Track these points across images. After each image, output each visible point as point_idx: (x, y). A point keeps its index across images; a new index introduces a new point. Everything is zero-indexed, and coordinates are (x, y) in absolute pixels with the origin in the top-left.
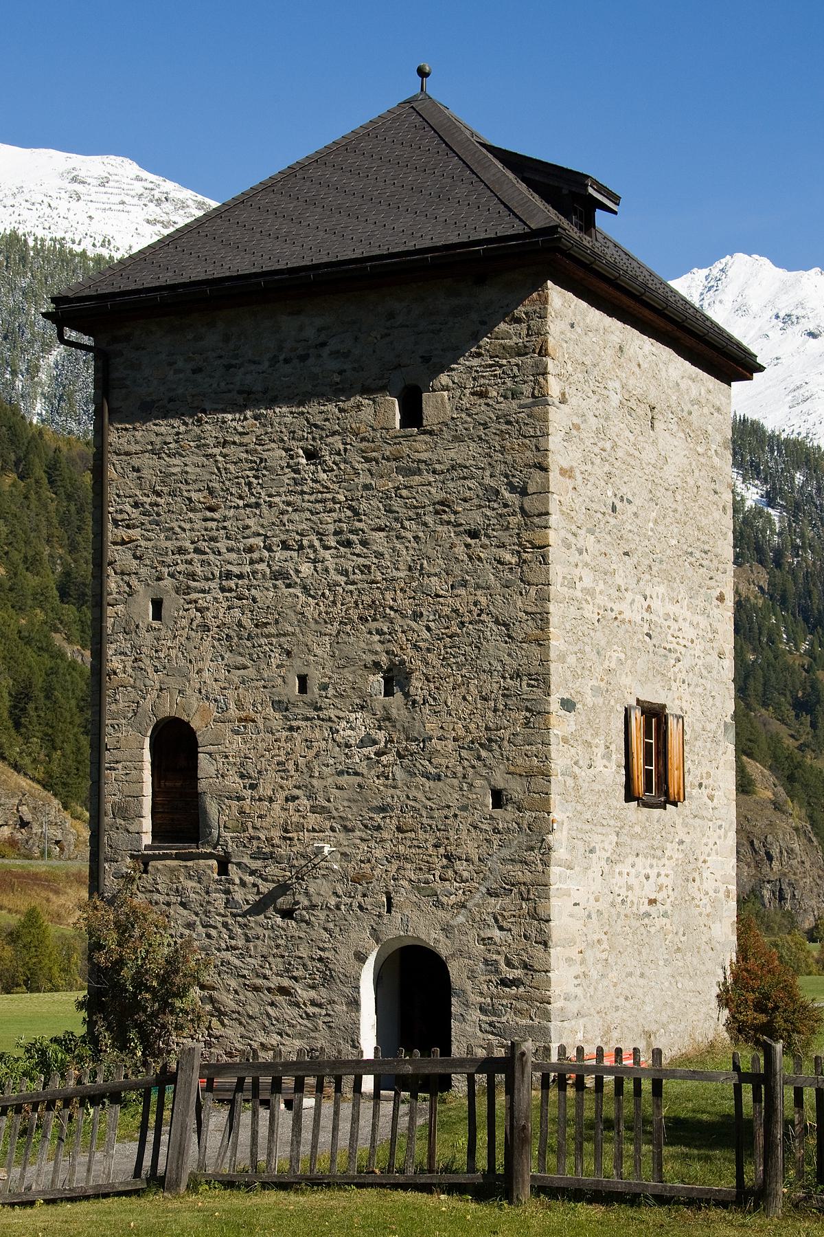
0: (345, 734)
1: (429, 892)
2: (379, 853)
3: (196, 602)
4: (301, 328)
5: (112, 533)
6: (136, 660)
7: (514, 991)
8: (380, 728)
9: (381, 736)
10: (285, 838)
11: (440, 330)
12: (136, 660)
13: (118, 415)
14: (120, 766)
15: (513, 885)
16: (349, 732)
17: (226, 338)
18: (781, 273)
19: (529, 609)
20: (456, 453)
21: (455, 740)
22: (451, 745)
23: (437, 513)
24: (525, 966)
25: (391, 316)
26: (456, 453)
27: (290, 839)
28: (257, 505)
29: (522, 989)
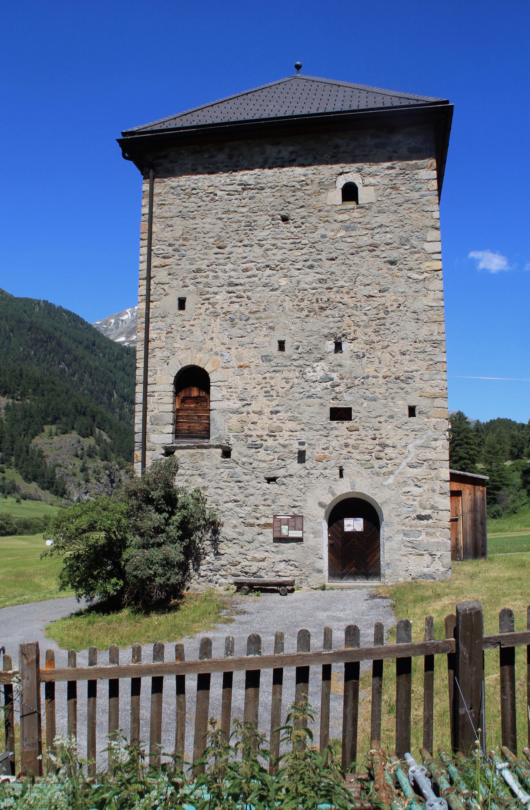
0: (310, 375)
1: (369, 466)
2: (334, 443)
3: (208, 299)
4: (279, 152)
5: (155, 261)
6: (168, 333)
7: (425, 522)
8: (334, 371)
9: (334, 375)
10: (270, 436)
11: (368, 155)
12: (168, 333)
13: (206, 434)
14: (156, 394)
15: (425, 461)
16: (312, 374)
17: (231, 157)
18: (184, 365)
19: (431, 304)
20: (382, 219)
21: (385, 377)
22: (381, 381)
23: (371, 251)
24: (432, 507)
25: (337, 147)
26: (382, 219)
27: (275, 436)
28: (251, 246)
29: (430, 521)
